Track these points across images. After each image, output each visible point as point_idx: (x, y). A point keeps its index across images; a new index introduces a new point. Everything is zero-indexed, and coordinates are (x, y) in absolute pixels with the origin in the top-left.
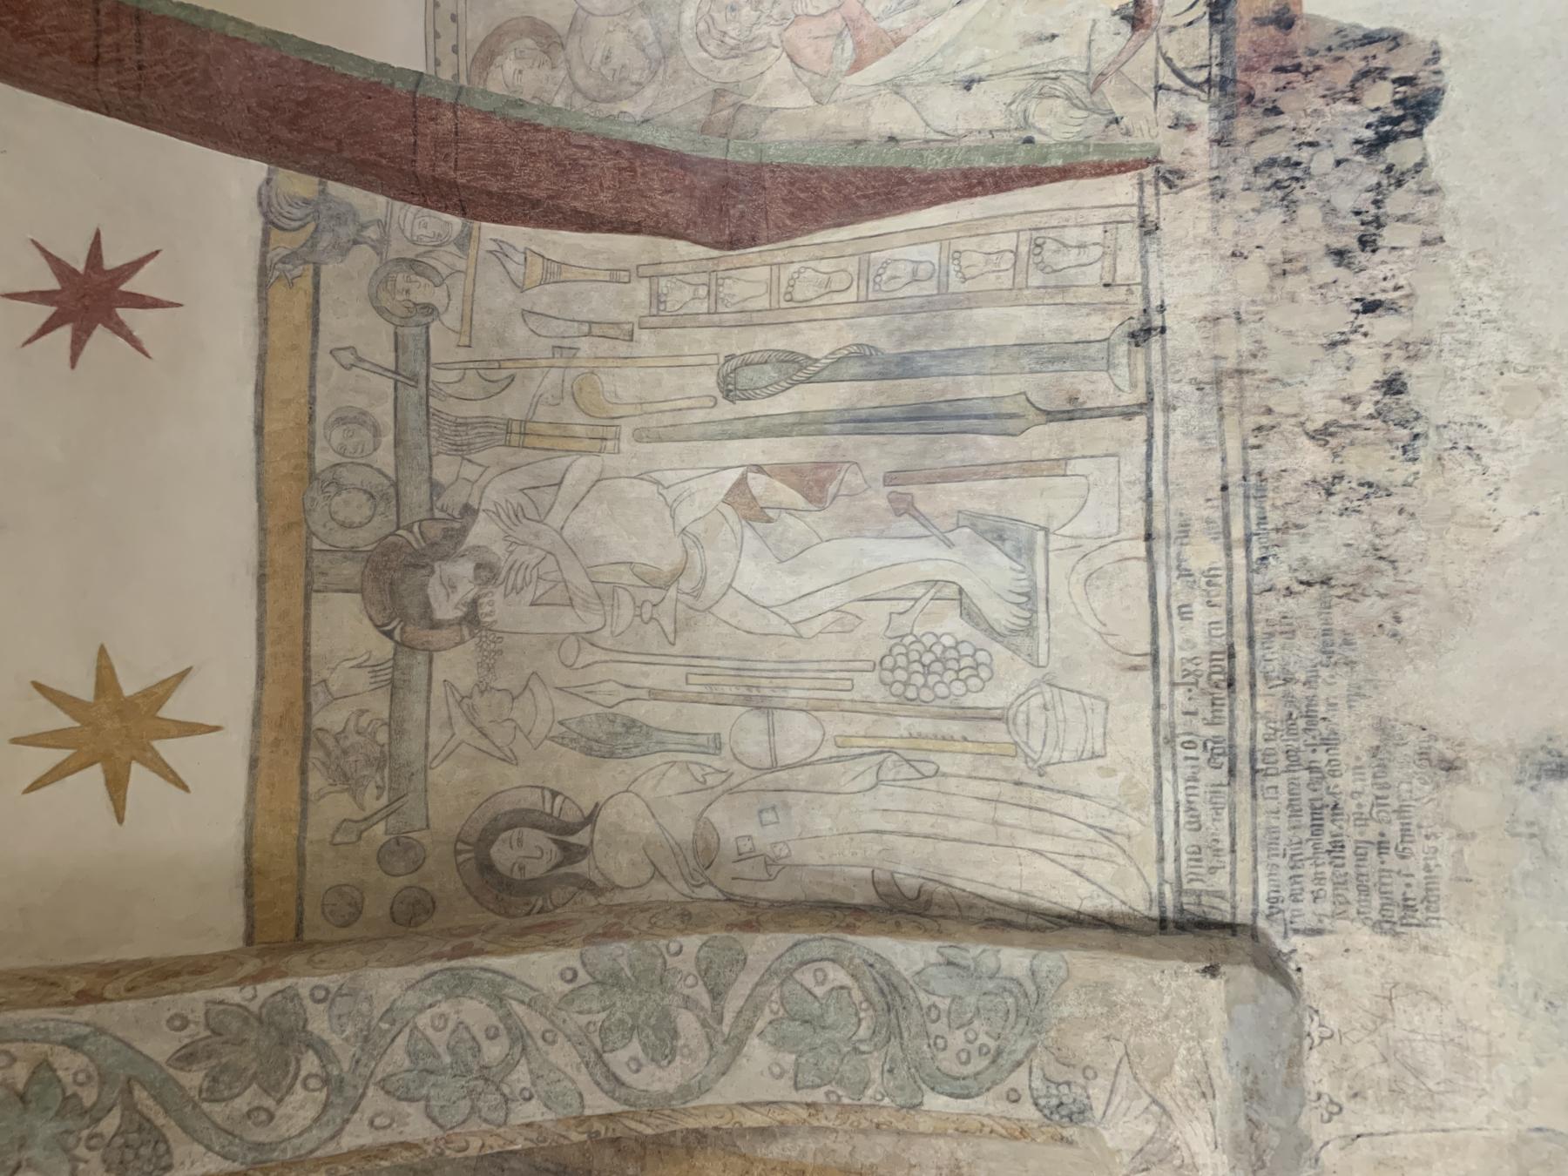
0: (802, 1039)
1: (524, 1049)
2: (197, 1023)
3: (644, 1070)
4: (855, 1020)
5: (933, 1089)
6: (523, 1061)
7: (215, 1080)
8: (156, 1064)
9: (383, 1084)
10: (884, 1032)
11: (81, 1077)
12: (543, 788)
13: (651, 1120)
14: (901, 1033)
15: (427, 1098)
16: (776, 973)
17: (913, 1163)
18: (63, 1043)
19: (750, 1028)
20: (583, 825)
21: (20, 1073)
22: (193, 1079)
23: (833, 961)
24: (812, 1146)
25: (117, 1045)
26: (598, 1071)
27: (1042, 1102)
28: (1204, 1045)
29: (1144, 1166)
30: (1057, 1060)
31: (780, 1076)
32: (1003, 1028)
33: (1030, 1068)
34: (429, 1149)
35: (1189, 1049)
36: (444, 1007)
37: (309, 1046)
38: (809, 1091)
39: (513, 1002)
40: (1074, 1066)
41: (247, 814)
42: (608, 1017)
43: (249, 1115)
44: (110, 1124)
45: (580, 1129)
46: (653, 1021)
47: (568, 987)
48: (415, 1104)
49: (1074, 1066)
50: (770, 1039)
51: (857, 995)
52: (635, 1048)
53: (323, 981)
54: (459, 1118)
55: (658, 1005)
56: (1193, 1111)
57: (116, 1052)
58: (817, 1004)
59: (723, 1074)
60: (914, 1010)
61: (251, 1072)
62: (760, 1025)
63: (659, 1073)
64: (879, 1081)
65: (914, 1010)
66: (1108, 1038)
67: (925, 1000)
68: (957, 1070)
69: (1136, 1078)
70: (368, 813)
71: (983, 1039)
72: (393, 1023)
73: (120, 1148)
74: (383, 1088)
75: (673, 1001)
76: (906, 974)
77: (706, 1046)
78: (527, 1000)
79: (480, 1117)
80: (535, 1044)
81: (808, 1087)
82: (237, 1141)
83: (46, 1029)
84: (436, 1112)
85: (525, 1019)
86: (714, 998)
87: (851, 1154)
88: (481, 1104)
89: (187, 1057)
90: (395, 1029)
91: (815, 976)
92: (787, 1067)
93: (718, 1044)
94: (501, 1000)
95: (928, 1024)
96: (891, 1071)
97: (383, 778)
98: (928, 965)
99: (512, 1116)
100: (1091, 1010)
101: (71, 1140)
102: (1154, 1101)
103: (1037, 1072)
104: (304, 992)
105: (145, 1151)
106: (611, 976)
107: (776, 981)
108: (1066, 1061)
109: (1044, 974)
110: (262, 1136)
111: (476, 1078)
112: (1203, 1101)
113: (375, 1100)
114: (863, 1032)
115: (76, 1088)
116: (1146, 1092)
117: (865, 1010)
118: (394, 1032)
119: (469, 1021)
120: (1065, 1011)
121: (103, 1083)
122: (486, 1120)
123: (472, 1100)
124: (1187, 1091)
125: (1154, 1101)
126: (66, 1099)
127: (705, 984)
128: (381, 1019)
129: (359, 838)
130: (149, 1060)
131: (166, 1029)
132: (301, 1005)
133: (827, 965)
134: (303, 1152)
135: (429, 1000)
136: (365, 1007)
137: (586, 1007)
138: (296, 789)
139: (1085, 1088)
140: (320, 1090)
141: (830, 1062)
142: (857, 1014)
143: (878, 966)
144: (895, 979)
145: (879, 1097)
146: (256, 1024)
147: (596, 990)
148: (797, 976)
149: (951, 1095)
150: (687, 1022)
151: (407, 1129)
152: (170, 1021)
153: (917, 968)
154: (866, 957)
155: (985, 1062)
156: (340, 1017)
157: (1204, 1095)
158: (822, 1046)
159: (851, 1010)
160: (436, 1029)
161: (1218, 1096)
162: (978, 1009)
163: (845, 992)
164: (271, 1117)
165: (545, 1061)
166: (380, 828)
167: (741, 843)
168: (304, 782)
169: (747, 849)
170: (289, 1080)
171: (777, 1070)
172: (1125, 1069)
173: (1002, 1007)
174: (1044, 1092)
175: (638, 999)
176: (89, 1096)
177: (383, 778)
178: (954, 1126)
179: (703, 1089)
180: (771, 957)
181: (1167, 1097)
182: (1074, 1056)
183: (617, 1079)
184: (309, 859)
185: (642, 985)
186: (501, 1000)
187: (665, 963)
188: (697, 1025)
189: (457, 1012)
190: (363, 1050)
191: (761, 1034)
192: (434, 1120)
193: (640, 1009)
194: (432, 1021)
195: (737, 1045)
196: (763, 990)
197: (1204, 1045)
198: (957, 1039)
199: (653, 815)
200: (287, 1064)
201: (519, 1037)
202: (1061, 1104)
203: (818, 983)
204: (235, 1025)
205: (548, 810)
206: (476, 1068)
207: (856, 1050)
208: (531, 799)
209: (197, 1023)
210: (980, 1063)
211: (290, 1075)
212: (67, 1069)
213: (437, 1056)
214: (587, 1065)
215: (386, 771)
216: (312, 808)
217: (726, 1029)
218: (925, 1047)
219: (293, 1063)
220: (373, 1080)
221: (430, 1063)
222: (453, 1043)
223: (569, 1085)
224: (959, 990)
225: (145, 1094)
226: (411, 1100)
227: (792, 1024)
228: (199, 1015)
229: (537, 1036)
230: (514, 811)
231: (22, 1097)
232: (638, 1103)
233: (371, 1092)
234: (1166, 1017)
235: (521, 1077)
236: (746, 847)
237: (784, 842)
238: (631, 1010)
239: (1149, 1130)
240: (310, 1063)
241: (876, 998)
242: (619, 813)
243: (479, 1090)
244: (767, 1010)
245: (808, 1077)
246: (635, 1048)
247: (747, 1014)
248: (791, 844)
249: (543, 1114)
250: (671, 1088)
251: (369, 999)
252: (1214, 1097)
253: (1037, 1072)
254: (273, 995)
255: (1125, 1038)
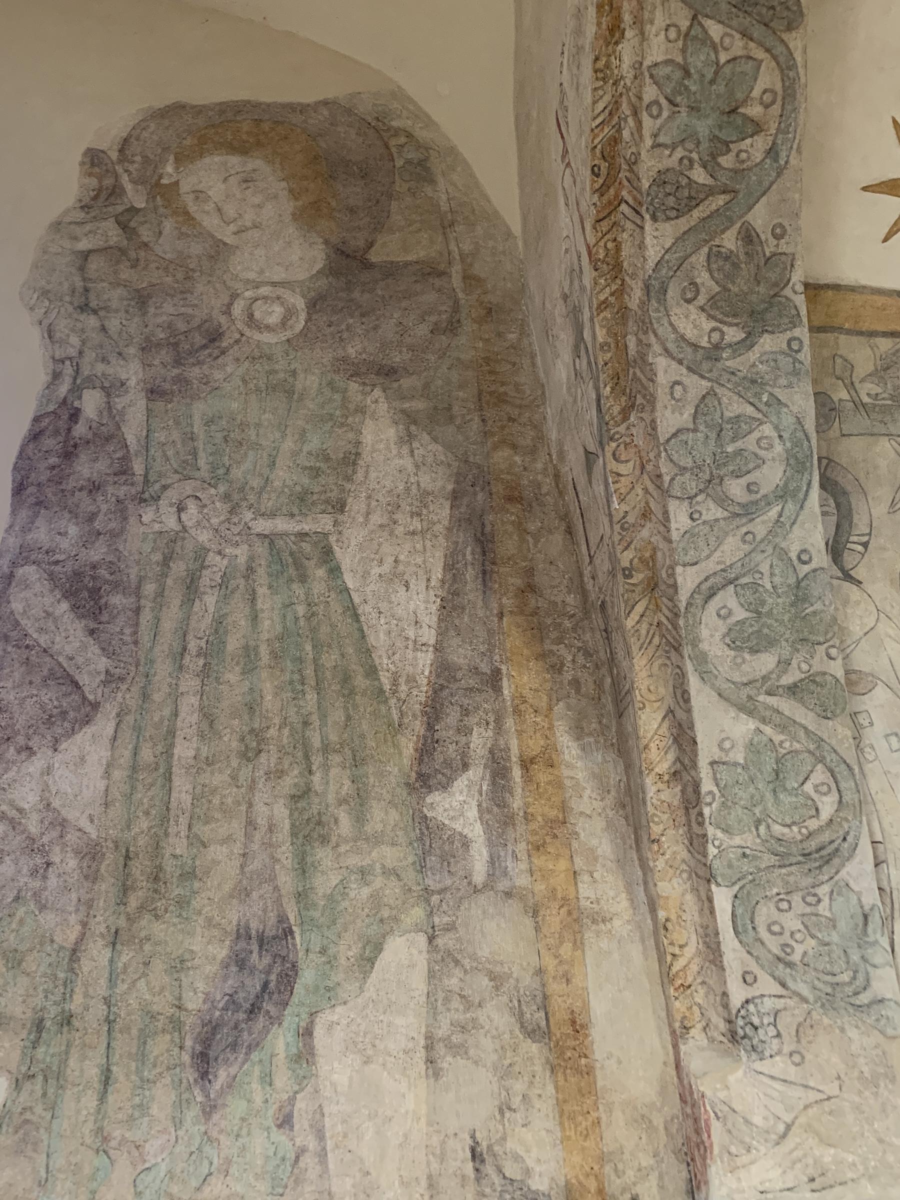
0: (759, 770)
1: (738, 515)
2: (777, 246)
3: (721, 622)
4: (789, 822)
5: (736, 897)
6: (726, 514)
7: (727, 258)
8: (746, 213)
9: (711, 393)
10: (782, 849)
11: (744, 156)
12: (870, 534)
13: (644, 627)
14: (785, 866)
15: (695, 430)
16: (818, 747)
17: (595, 875)
18: (774, 143)
19: (763, 721)
20: (842, 569)
21: (754, 111)
22: (730, 241)
23: (840, 802)
24: (580, 776)
25: (766, 184)
26: (718, 580)
27: (751, 1007)
28: (864, 1181)
29: (720, 1114)
30: (799, 1025)
31: (720, 747)
32: (815, 969)
33: (781, 997)
34: (622, 429)
35: (854, 1164)
36: (778, 448)
37: (749, 334)
38: (711, 775)
39: (780, 507)
40: (799, 1041)
41: (864, 287)
42: (766, 591)
43: (693, 284)
44: (699, 175)
45: (636, 560)
46: (766, 631)
47: (793, 555)
48: (691, 419)
49: (799, 1041)
50: (756, 739)
51: (813, 824)
52: (740, 614)
53: (806, 348)
54: (675, 457)
55: (781, 636)
56: (792, 1168)
57: (760, 183)
58: (796, 785)
59: (720, 695)
60: (810, 880)
61: (730, 286)
62: (768, 730)
63: (718, 635)
64: (732, 843)
65: (810, 880)
66: (839, 1078)
67: (823, 891)
68: (761, 921)
69: (806, 1107)
70: (857, 385)
71: (799, 949)
72: (767, 404)
73: (678, 182)
74: (708, 393)
75: (786, 651)
76: (843, 873)
77: (745, 680)
78: (782, 519)
79: (676, 475)
80: (743, 525)
81: (715, 774)
82: (671, 273)
83: (788, 133)
84: (683, 437)
85: (765, 518)
86: (789, 688)
87: (582, 813)
88: (688, 475)
89: (749, 237)
90: (762, 407)
91: (823, 784)
92: (731, 755)
93: (747, 690)
94: (781, 497)
95: (800, 894)
96: (744, 855)
97: (883, 399)
98: (859, 895)
99: (677, 502)
100: (862, 1060)
101: (690, 145)
102: (788, 1127)
103: (780, 1003)
104: (797, 332)
105: (671, 201)
106: (805, 594)
107: (812, 747)
108: (801, 1034)
109: (883, 1013)
110: (673, 292)
111: (711, 473)
112: (806, 1179)
113: (697, 386)
114: (777, 829)
115: (736, 151)
116: (796, 1118)
117: (800, 832)
118: (758, 405)
119: (765, 469)
120: (853, 1033)
121: (736, 171)
122: (673, 479)
123: (692, 469)
124: (810, 1161)
125: (788, 1127)
126: (727, 144)
127: (802, 680)
128: (771, 394)
129: (838, 378)
130: (750, 208)
131: (775, 221)
132: (786, 330)
133: (834, 797)
134: (656, 326)
135: (786, 435)
136: (783, 381)
137: (777, 571)
138: (881, 328)
139: (779, 1053)
140: (709, 342)
141: (744, 795)
142: (794, 823)
143: (846, 845)
144: (836, 861)
145: (717, 843)
146: (772, 293)
147: (792, 580)
148: (820, 767)
149: (733, 915)
150: (766, 662)
151: (668, 413)
152: (781, 225)
153: (852, 884)
154: (852, 834)
155: (776, 951)
156: (776, 361)
157: (812, 1180)
158: (757, 789)
159: (797, 818)
160: (759, 441)
161: (816, 1195)
162: (827, 944)
163: (814, 812)
164: (689, 301)
165: (727, 534)
166: (844, 395)
167: (864, 715)
168: (885, 334)
169: (862, 721)
170: (720, 316)
171: (727, 745)
172: (813, 1096)
173: (836, 969)
174: (763, 1011)
175: (786, 618)
176: (726, 161)
177: (883, 399)
178: (673, 917)
179: (704, 675)
180: (833, 742)
181: (798, 1140)
182: (810, 1042)
183: (711, 596)
184: (822, 336)
185: (798, 623)
186: (781, 497)
187: (819, 643)
188: (764, 672)
189: (773, 459)
190: (744, 378)
191: (759, 731)
192: (675, 435)
193: (777, 621)
194: (766, 437)
195: (748, 708)
196: (802, 733)
197: (864, 1181)
198: (791, 922)
199: (866, 634)
200: (735, 316)
201: (748, 511)
202: (756, 1028)
203: (816, 787)
204: (773, 276)
205: (852, 539)
206: (722, 473)
207: (758, 823)
208: (861, 524)
209: (777, 246)
210: (773, 944)
211: (725, 319)
212: (752, 146)
213: (734, 439)
214: (723, 570)
215: (889, 402)
216: (862, 339)
217: (761, 698)
218: (775, 890)
219: (735, 321)
220: (715, 385)
221: (728, 434)
222: (746, 454)
223: (704, 554)
224: (842, 925)
225: (721, 203)
226: (695, 417)
227: (773, 760)
228: (783, 248)
229: (750, 527)
230: (851, 509)
231: (733, 111)
232: (689, 615)
233: (705, 383)
234: (881, 1141)
235: (712, 511)
236: (863, 720)
237: (877, 756)
238: (775, 611)
239: (757, 1120)
240: (733, 334)
241: (813, 844)
242: (858, 603)
243: (700, 475)
244: (782, 737)
245: (724, 775)
246: (740, 614)
247: (777, 719)
248: (876, 763)
249: (677, 529)
250: (704, 646)
251: (790, 386)
252: (813, 1191)
253: (780, 1003)
254: (796, 307)
255: (845, 1096)
